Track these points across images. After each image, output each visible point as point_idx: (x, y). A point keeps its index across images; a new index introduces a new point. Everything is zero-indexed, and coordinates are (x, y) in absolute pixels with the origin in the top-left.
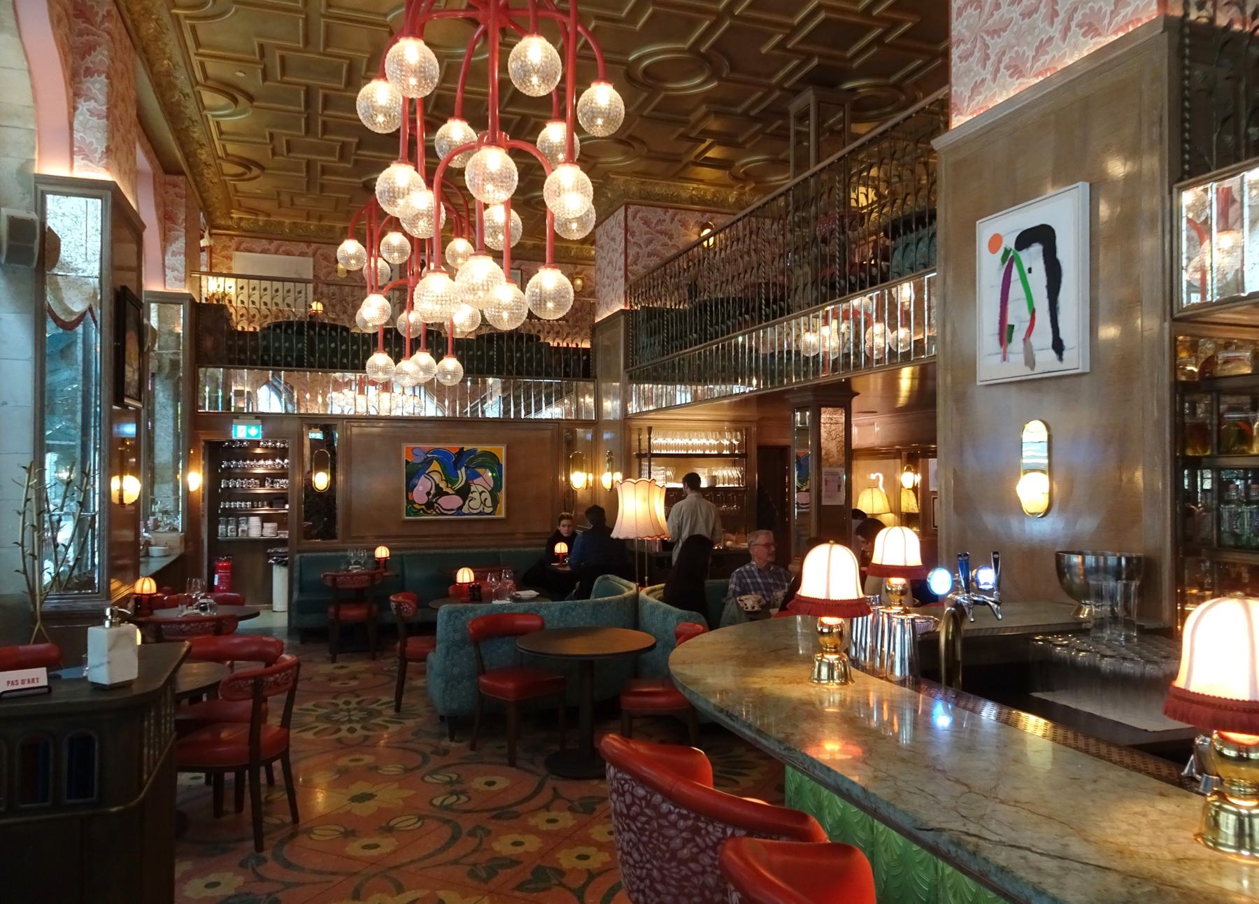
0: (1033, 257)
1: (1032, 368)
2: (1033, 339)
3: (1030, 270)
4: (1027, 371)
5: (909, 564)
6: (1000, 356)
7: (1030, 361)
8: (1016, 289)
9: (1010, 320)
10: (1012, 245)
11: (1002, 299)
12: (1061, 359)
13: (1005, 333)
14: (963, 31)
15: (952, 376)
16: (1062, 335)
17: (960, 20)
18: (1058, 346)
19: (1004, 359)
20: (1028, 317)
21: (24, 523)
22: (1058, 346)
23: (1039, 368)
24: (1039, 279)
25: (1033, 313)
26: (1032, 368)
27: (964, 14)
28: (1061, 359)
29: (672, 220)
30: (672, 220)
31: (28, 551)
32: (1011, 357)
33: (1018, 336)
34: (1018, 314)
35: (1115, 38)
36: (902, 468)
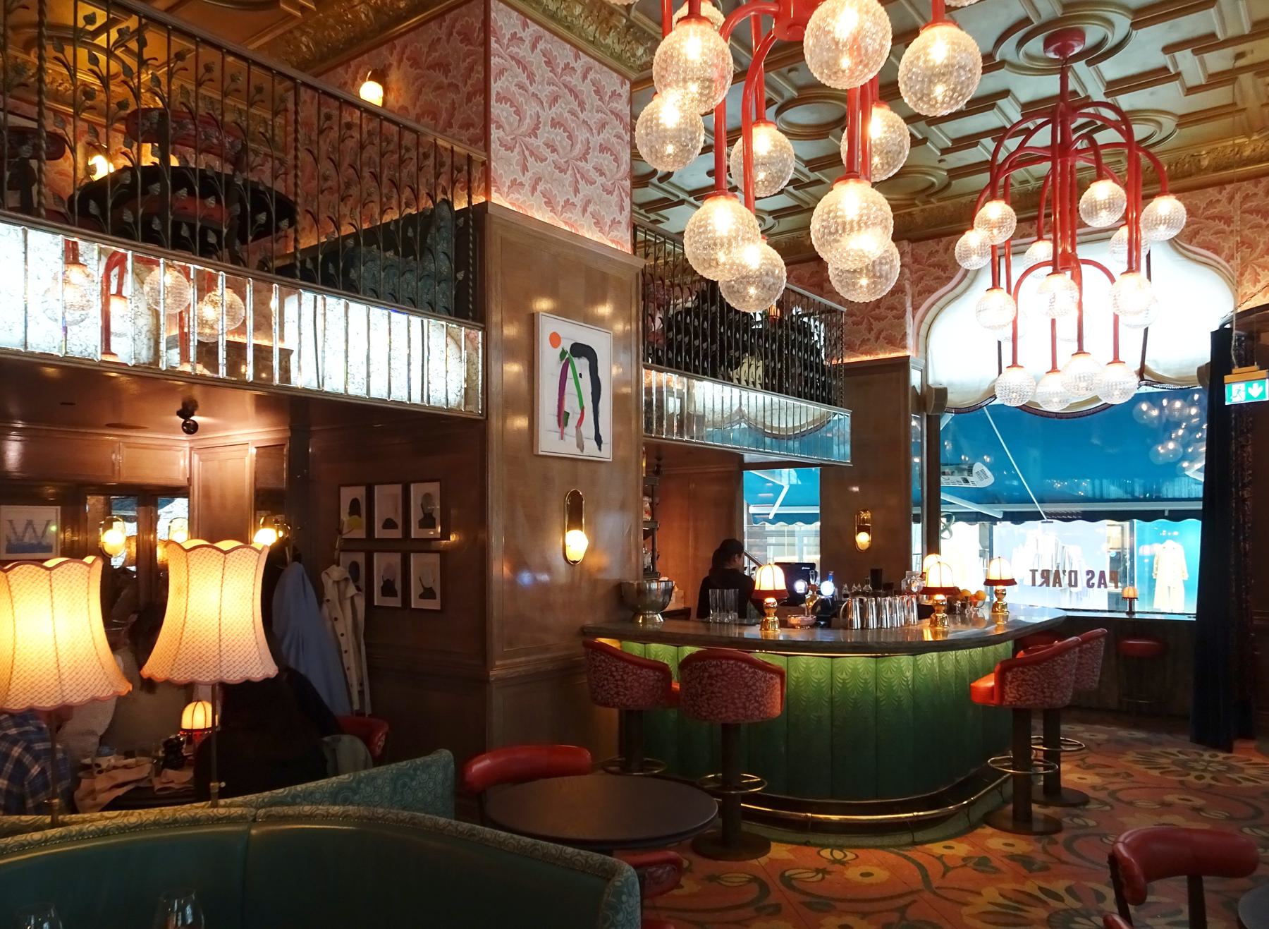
0: (582, 364)
1: (582, 451)
2: (582, 428)
3: (581, 375)
4: (578, 451)
5: (777, 588)
6: (558, 435)
7: (581, 446)
8: (570, 383)
9: (566, 409)
10: (568, 349)
11: (593, 394)
12: (600, 449)
13: (563, 418)
14: (473, 116)
15: (1097, 445)
16: (601, 433)
17: (470, 105)
18: (598, 439)
19: (562, 438)
20: (580, 411)
21: (1098, 864)
22: (598, 439)
23: (586, 452)
24: (586, 383)
25: (582, 409)
26: (582, 451)
27: (474, 100)
28: (600, 449)
29: (1231, 199)
30: (1231, 199)
31: (78, 688)
32: (566, 437)
33: (572, 422)
34: (571, 405)
35: (510, 207)
36: (256, 521)
